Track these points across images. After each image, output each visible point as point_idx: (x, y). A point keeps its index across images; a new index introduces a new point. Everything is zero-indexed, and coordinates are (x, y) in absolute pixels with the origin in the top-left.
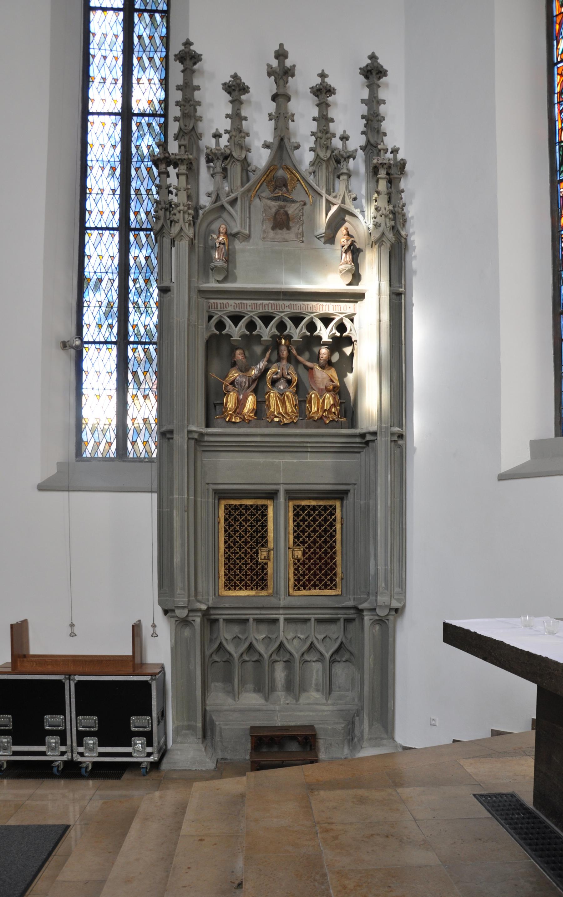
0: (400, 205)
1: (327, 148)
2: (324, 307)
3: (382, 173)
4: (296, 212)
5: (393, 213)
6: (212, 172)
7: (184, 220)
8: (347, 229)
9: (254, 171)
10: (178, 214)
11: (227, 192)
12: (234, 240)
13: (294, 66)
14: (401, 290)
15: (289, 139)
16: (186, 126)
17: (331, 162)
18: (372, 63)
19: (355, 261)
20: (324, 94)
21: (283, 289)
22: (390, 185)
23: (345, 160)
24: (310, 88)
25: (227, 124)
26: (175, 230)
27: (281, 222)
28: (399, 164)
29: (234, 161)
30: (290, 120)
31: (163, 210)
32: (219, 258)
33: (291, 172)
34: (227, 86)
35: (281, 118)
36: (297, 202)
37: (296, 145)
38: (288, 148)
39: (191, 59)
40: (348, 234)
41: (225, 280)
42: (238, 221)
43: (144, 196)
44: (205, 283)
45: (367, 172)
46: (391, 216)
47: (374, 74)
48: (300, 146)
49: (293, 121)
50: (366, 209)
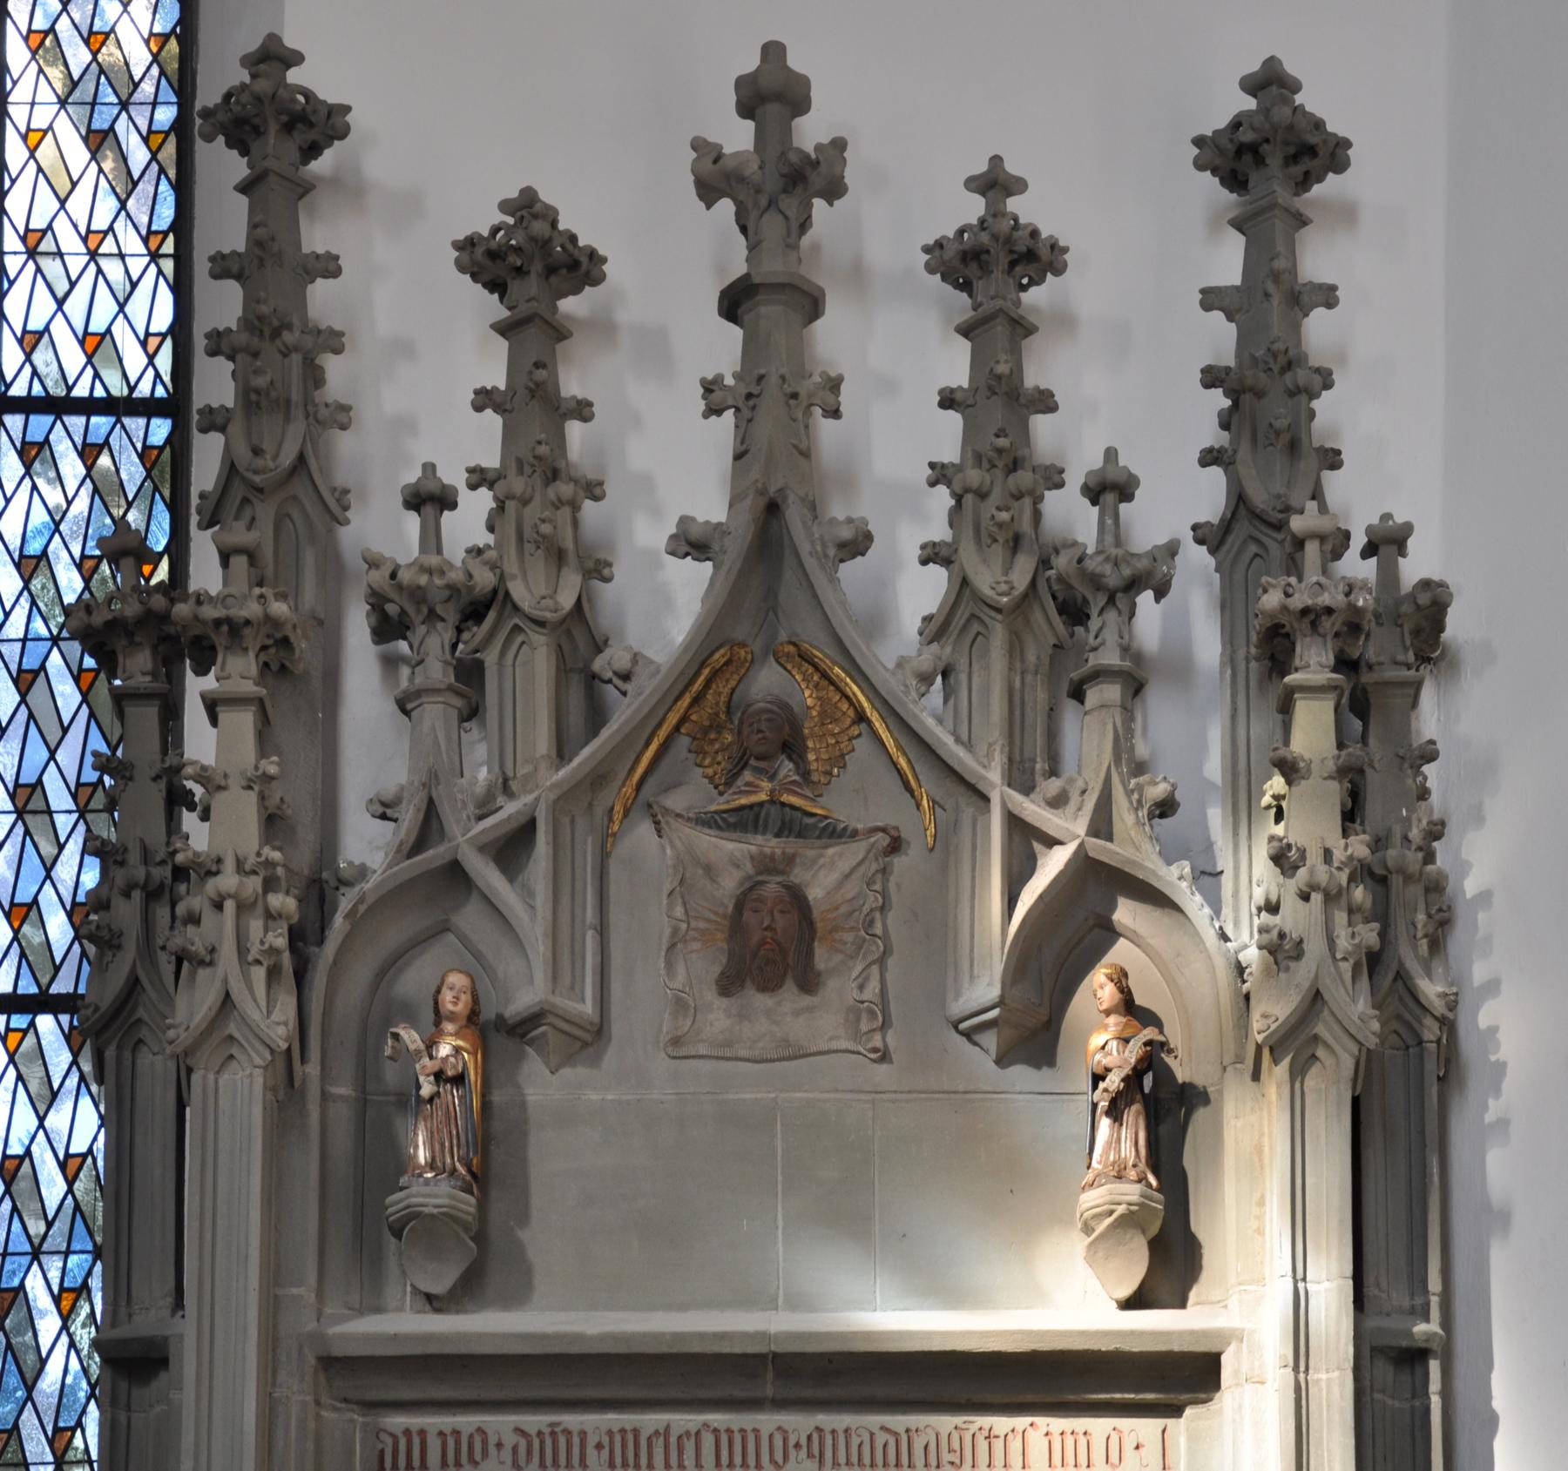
0: (1415, 834)
1: (1016, 544)
2: (998, 1445)
3: (1314, 663)
4: (851, 889)
5: (1372, 875)
6: (404, 684)
7: (242, 950)
8: (1120, 979)
9: (626, 677)
10: (208, 916)
11: (480, 789)
12: (521, 1056)
13: (839, 145)
14: (1420, 1328)
15: (813, 507)
16: (257, 452)
17: (1037, 616)
18: (1264, 110)
19: (1166, 1160)
20: (998, 274)
21: (778, 1337)
22: (1357, 724)
23: (1111, 601)
24: (927, 249)
25: (483, 440)
26: (193, 1005)
27: (770, 948)
28: (1407, 608)
29: (517, 629)
30: (818, 411)
31: (137, 895)
32: (432, 1165)
33: (825, 675)
34: (479, 251)
35: (775, 404)
36: (855, 833)
37: (846, 534)
38: (805, 548)
39: (288, 128)
40: (1127, 1005)
41: (468, 1290)
42: (539, 950)
43: (64, 822)
44: (361, 1312)
45: (1229, 658)
46: (1359, 893)
47: (1274, 161)
48: (868, 537)
49: (835, 413)
50: (1224, 862)
